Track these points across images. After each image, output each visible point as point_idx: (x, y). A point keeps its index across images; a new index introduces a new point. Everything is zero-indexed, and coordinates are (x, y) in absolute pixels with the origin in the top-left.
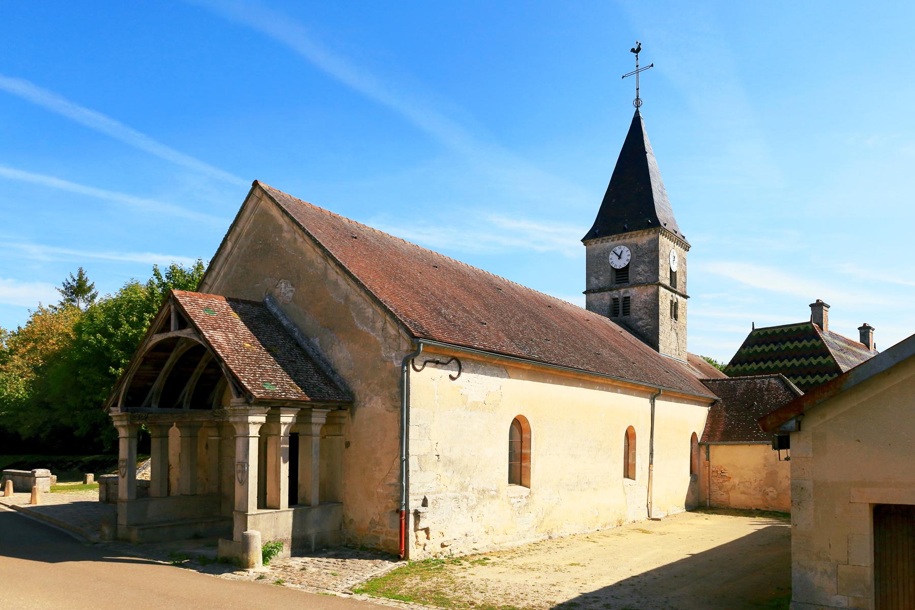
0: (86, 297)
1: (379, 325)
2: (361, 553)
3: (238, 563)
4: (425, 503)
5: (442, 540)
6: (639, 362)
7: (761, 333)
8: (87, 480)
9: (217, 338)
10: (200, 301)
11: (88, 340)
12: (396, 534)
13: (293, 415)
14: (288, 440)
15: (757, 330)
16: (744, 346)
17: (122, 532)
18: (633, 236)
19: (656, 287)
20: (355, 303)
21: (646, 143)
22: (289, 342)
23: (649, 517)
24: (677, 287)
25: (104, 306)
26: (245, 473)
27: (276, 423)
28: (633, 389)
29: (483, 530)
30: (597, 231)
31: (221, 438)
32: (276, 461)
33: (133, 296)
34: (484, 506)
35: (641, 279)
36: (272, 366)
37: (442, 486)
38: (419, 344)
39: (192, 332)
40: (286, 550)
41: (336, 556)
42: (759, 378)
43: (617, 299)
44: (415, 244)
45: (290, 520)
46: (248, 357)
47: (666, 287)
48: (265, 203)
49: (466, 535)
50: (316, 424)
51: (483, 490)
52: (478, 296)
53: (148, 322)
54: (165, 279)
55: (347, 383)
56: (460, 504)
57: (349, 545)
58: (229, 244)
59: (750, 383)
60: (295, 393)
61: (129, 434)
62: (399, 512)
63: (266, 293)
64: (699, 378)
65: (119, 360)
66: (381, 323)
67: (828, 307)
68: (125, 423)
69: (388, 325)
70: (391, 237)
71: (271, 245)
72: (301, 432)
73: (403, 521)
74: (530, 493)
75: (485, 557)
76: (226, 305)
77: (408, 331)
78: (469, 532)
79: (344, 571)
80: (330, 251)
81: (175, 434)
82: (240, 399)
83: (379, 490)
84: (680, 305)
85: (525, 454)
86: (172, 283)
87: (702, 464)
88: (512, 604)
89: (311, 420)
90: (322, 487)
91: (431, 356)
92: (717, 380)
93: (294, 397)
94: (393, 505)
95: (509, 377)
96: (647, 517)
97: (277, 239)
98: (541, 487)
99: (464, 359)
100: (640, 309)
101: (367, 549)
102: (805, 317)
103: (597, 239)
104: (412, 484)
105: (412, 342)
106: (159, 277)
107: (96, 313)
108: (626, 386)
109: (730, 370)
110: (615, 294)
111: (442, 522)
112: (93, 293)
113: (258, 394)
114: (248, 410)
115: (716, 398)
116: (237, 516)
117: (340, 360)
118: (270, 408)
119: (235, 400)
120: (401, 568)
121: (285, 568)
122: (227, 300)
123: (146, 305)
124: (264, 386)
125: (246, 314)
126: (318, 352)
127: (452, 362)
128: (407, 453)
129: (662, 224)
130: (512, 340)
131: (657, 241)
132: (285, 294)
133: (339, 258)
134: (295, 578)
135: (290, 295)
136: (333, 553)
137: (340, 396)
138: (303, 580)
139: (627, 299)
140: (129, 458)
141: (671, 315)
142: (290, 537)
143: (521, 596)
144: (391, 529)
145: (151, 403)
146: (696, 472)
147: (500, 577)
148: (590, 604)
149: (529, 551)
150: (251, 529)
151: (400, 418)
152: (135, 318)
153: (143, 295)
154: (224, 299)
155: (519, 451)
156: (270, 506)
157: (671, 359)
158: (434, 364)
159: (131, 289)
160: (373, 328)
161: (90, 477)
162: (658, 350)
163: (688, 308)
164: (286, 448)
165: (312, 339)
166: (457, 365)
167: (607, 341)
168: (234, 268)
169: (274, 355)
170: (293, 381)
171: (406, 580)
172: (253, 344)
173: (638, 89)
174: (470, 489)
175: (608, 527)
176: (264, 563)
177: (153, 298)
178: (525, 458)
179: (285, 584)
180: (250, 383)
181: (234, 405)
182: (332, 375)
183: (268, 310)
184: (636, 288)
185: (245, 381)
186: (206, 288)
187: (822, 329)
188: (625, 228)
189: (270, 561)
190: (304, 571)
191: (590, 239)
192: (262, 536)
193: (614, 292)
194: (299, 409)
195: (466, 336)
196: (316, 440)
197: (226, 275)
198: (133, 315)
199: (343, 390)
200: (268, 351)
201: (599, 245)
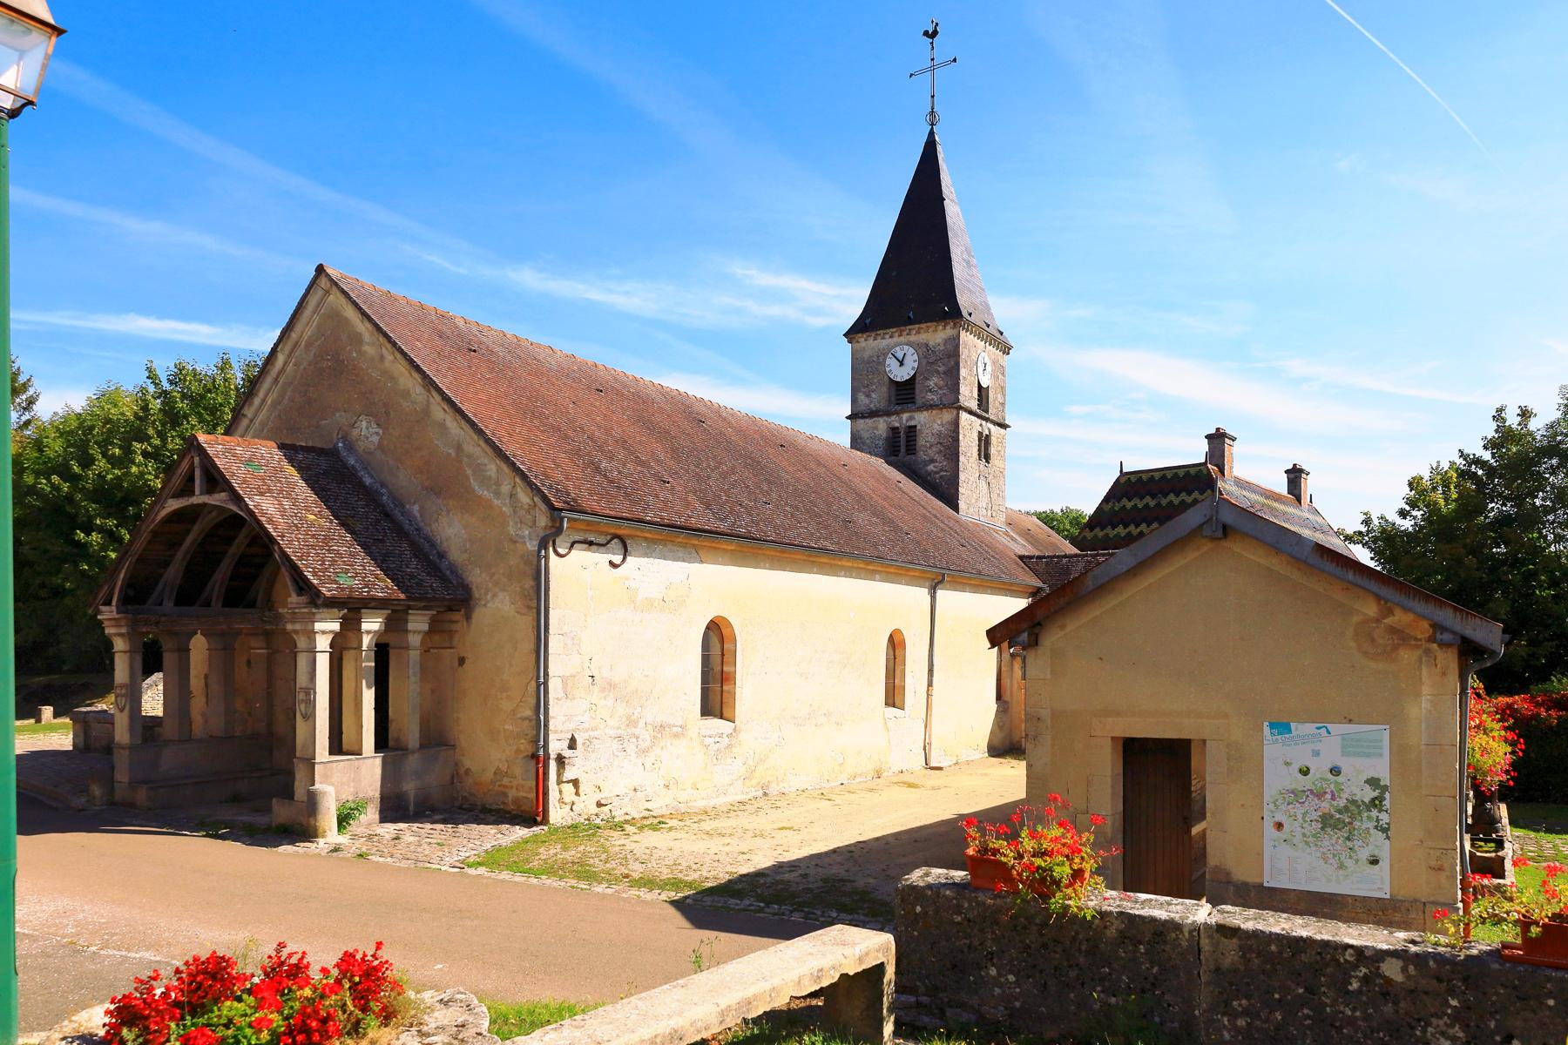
0: (18, 400)
1: (505, 489)
2: (482, 816)
3: (300, 830)
4: (572, 744)
5: (598, 796)
6: (917, 531)
7: (1133, 479)
8: (43, 717)
9: (267, 507)
10: (239, 451)
11: (34, 486)
12: (531, 788)
13: (380, 620)
14: (373, 655)
15: (1127, 473)
16: (1107, 499)
17: (121, 792)
18: (922, 331)
19: (955, 412)
20: (470, 456)
21: (944, 184)
22: (374, 510)
23: (927, 764)
24: (990, 411)
25: (61, 427)
26: (311, 704)
27: (356, 632)
28: (901, 574)
29: (662, 782)
30: (868, 321)
31: (270, 651)
32: (356, 686)
33: (112, 411)
34: (662, 748)
35: (933, 399)
36: (349, 548)
37: (598, 721)
38: (562, 519)
39: (228, 498)
40: (372, 814)
41: (444, 822)
42: (1104, 555)
43: (898, 428)
44: (569, 353)
45: (378, 771)
46: (313, 536)
47: (971, 412)
48: (335, 298)
49: (635, 789)
50: (415, 632)
51: (661, 726)
52: (663, 435)
53: (140, 457)
54: (166, 386)
55: (460, 572)
56: (625, 745)
57: (464, 806)
58: (281, 358)
59: (1090, 562)
60: (383, 589)
61: (131, 647)
62: (535, 757)
63: (338, 434)
64: (1020, 553)
65: (91, 519)
66: (509, 486)
67: (1234, 439)
68: (123, 630)
69: (519, 489)
70: (532, 344)
71: (346, 362)
72: (392, 644)
73: (541, 770)
74: (735, 729)
75: (661, 819)
76: (277, 455)
77: (545, 499)
78: (640, 785)
79: (456, 839)
80: (434, 378)
81: (199, 646)
82: (303, 597)
83: (507, 727)
84: (994, 440)
85: (729, 673)
86: (178, 392)
87: (1016, 686)
88: (680, 875)
89: (407, 626)
90: (425, 724)
91: (581, 534)
92: (1044, 557)
93: (381, 594)
94: (527, 748)
95: (702, 562)
96: (924, 764)
97: (355, 355)
98: (752, 721)
99: (632, 537)
100: (931, 446)
101: (490, 811)
102: (1194, 452)
103: (867, 334)
104: (553, 717)
105: (552, 516)
106: (157, 381)
107: (47, 437)
108: (887, 570)
109: (1085, 537)
110: (895, 421)
111: (599, 771)
112: (31, 393)
113: (329, 591)
114: (314, 614)
115: (1040, 584)
116: (301, 765)
117: (450, 537)
118: (346, 611)
119: (294, 599)
120: (536, 835)
121: (370, 837)
122: (279, 448)
123: (136, 428)
124: (337, 579)
125: (308, 468)
126: (417, 525)
127: (613, 542)
128: (546, 674)
129: (965, 313)
130: (708, 506)
131: (957, 341)
132: (367, 438)
133: (448, 388)
134: (385, 850)
135: (375, 439)
136: (442, 817)
137: (450, 592)
138: (395, 852)
139: (912, 430)
140: (131, 681)
141: (979, 455)
142: (377, 795)
143: (694, 867)
144: (523, 782)
145: (162, 600)
146: (1006, 697)
147: (672, 844)
148: (784, 873)
149: (727, 812)
150: (321, 783)
151: (535, 624)
152: (117, 450)
153: (129, 410)
154: (275, 445)
155: (719, 668)
156: (349, 748)
157: (977, 524)
158: (586, 546)
159: (108, 398)
160: (498, 494)
161: (47, 711)
162: (956, 509)
163: (1007, 444)
164: (371, 667)
165: (408, 507)
166: (621, 546)
167: (871, 498)
168: (288, 393)
169: (352, 532)
170: (381, 570)
171: (541, 850)
172: (319, 515)
173: (933, 97)
174: (641, 724)
175: (858, 780)
176: (339, 830)
177: (146, 417)
178: (727, 679)
179: (369, 857)
180: (317, 575)
181: (294, 606)
182: (438, 561)
183: (342, 461)
184: (925, 413)
185: (309, 572)
186: (241, 428)
187: (1223, 475)
188: (909, 317)
189: (349, 828)
190: (397, 841)
191: (859, 333)
192: (336, 793)
193: (893, 418)
194: (390, 612)
195: (634, 503)
196: (414, 655)
197: (275, 405)
198: (112, 443)
199: (454, 582)
200: (343, 524)
201: (872, 344)
